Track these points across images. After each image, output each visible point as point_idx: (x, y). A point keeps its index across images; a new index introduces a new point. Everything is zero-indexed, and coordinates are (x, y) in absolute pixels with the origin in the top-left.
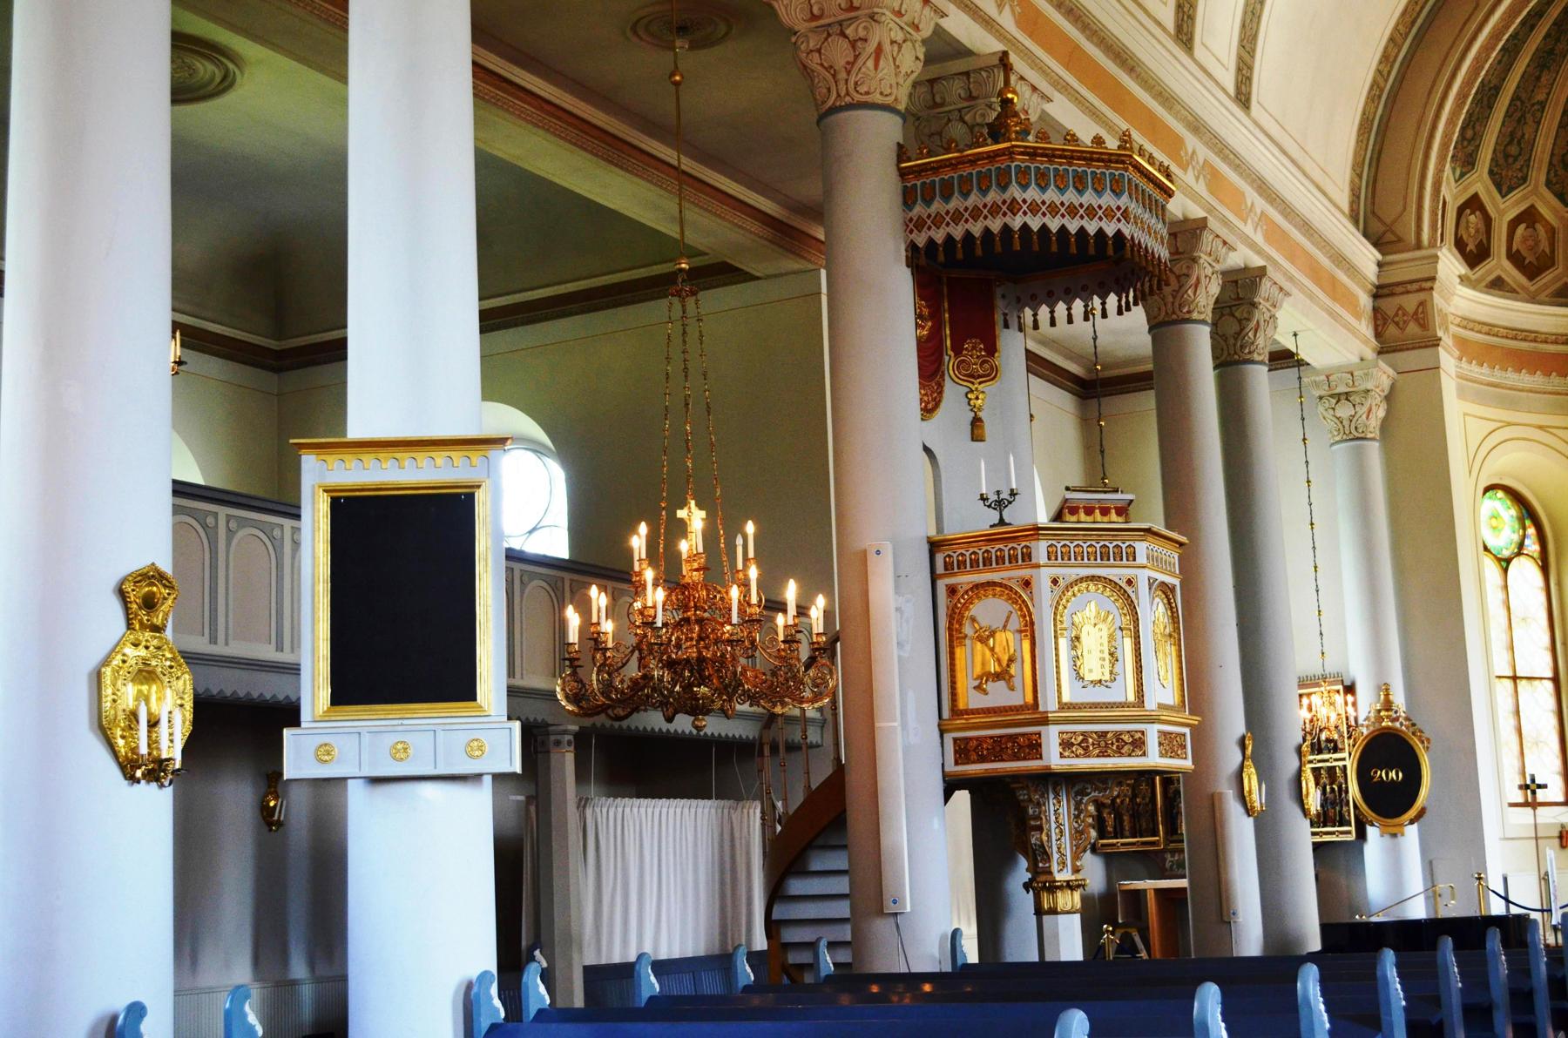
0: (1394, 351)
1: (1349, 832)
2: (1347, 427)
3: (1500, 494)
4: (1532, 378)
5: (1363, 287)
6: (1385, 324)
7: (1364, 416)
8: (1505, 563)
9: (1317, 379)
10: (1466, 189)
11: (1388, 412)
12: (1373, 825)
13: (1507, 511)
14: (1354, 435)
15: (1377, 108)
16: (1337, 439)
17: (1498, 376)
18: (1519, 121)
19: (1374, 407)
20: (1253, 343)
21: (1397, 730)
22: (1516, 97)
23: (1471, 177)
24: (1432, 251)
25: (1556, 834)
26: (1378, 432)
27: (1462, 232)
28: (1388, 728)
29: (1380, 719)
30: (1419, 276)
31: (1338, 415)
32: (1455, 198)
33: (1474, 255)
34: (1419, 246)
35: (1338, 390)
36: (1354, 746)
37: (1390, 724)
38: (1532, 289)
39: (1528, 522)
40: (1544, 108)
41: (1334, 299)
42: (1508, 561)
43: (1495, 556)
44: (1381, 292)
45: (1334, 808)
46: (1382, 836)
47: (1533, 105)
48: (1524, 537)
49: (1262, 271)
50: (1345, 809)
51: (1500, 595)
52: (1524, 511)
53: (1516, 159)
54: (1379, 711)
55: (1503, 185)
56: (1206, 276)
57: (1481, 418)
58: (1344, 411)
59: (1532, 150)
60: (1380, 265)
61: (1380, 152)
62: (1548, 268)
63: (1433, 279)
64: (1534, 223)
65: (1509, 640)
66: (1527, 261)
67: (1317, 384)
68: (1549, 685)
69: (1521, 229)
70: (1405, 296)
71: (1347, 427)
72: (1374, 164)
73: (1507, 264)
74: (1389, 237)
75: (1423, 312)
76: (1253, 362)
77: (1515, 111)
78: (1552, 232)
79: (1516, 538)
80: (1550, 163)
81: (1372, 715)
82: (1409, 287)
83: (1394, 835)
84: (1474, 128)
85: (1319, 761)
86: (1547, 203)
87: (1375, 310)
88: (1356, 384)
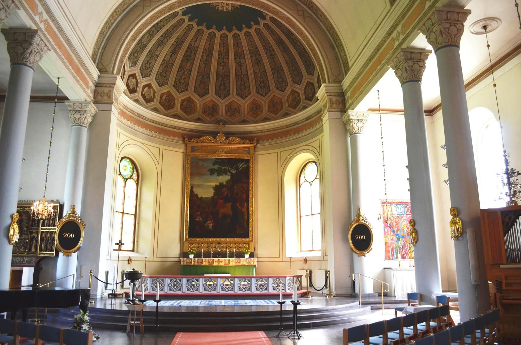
0: (98, 103)
1: (53, 254)
2: (77, 121)
3: (128, 160)
4: (142, 129)
5: (92, 81)
6: (97, 95)
7: (83, 119)
8: (126, 180)
9: (70, 104)
10: (132, 71)
11: (93, 120)
12: (61, 252)
13: (129, 166)
14: (79, 124)
15: (108, 31)
16: (73, 124)
17: (132, 125)
18: (150, 58)
19: (87, 117)
20: (28, 58)
21: (75, 220)
22: (150, 51)
23: (133, 68)
24: (116, 76)
25: (127, 259)
26: (88, 125)
27: (129, 82)
28: (72, 220)
29: (70, 216)
30: (110, 82)
31: (75, 117)
32: (129, 72)
33: (132, 90)
34: (113, 73)
35: (76, 109)
36: (59, 224)
37: (73, 218)
38: (147, 106)
39: (135, 170)
40: (158, 57)
41: (77, 74)
42: (127, 179)
43: (123, 177)
44: (98, 85)
45: (50, 245)
46: (63, 256)
47: (155, 55)
48: (133, 174)
49: (36, 32)
50: (53, 246)
51: (123, 189)
52: (134, 167)
53: (148, 69)
54: (70, 214)
55: (144, 75)
56: (35, 52)
57: (125, 135)
58: (77, 116)
59: (153, 68)
60: (99, 77)
61: (106, 45)
62: (152, 102)
63: (115, 84)
64: (150, 88)
65: (123, 201)
66: (146, 98)
67: (70, 106)
68: (133, 217)
69: (146, 88)
70: (105, 88)
71: (77, 121)
72: (104, 48)
73: (141, 97)
74: (104, 70)
75: (110, 94)
76: (27, 65)
77: (150, 55)
78: (154, 92)
79: (131, 174)
80: (157, 74)
81: (67, 215)
82: (107, 85)
83: (68, 256)
84: (137, 54)
85: (48, 229)
86: (154, 84)
87: (95, 90)
88: (83, 108)
